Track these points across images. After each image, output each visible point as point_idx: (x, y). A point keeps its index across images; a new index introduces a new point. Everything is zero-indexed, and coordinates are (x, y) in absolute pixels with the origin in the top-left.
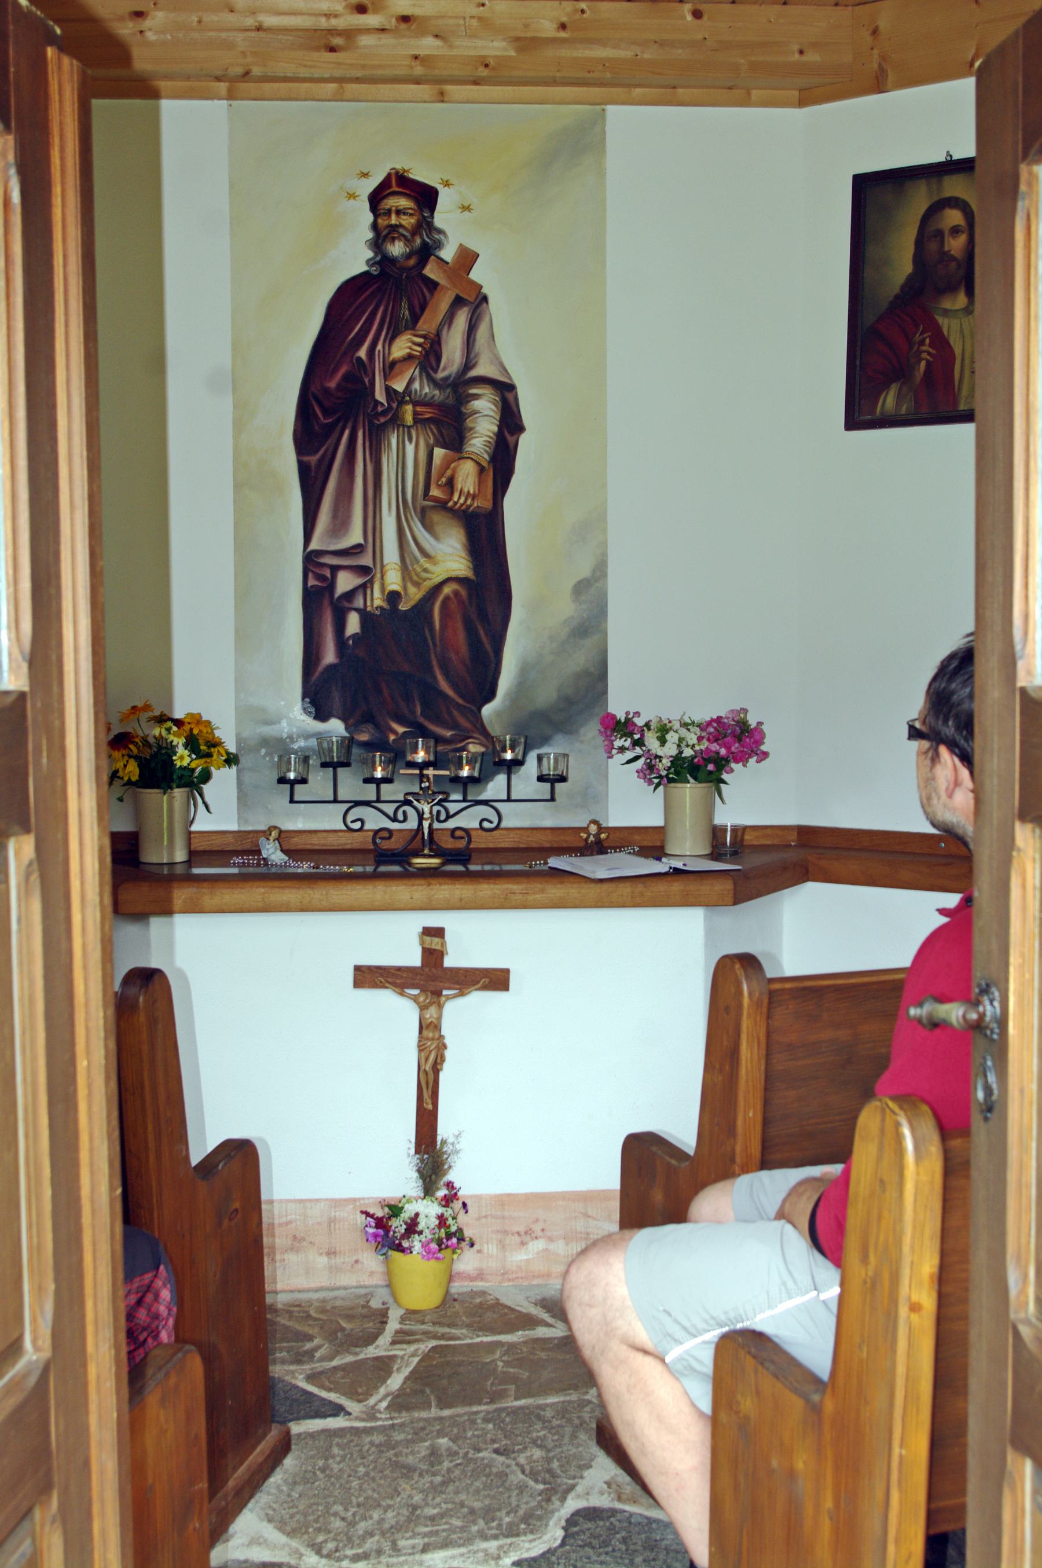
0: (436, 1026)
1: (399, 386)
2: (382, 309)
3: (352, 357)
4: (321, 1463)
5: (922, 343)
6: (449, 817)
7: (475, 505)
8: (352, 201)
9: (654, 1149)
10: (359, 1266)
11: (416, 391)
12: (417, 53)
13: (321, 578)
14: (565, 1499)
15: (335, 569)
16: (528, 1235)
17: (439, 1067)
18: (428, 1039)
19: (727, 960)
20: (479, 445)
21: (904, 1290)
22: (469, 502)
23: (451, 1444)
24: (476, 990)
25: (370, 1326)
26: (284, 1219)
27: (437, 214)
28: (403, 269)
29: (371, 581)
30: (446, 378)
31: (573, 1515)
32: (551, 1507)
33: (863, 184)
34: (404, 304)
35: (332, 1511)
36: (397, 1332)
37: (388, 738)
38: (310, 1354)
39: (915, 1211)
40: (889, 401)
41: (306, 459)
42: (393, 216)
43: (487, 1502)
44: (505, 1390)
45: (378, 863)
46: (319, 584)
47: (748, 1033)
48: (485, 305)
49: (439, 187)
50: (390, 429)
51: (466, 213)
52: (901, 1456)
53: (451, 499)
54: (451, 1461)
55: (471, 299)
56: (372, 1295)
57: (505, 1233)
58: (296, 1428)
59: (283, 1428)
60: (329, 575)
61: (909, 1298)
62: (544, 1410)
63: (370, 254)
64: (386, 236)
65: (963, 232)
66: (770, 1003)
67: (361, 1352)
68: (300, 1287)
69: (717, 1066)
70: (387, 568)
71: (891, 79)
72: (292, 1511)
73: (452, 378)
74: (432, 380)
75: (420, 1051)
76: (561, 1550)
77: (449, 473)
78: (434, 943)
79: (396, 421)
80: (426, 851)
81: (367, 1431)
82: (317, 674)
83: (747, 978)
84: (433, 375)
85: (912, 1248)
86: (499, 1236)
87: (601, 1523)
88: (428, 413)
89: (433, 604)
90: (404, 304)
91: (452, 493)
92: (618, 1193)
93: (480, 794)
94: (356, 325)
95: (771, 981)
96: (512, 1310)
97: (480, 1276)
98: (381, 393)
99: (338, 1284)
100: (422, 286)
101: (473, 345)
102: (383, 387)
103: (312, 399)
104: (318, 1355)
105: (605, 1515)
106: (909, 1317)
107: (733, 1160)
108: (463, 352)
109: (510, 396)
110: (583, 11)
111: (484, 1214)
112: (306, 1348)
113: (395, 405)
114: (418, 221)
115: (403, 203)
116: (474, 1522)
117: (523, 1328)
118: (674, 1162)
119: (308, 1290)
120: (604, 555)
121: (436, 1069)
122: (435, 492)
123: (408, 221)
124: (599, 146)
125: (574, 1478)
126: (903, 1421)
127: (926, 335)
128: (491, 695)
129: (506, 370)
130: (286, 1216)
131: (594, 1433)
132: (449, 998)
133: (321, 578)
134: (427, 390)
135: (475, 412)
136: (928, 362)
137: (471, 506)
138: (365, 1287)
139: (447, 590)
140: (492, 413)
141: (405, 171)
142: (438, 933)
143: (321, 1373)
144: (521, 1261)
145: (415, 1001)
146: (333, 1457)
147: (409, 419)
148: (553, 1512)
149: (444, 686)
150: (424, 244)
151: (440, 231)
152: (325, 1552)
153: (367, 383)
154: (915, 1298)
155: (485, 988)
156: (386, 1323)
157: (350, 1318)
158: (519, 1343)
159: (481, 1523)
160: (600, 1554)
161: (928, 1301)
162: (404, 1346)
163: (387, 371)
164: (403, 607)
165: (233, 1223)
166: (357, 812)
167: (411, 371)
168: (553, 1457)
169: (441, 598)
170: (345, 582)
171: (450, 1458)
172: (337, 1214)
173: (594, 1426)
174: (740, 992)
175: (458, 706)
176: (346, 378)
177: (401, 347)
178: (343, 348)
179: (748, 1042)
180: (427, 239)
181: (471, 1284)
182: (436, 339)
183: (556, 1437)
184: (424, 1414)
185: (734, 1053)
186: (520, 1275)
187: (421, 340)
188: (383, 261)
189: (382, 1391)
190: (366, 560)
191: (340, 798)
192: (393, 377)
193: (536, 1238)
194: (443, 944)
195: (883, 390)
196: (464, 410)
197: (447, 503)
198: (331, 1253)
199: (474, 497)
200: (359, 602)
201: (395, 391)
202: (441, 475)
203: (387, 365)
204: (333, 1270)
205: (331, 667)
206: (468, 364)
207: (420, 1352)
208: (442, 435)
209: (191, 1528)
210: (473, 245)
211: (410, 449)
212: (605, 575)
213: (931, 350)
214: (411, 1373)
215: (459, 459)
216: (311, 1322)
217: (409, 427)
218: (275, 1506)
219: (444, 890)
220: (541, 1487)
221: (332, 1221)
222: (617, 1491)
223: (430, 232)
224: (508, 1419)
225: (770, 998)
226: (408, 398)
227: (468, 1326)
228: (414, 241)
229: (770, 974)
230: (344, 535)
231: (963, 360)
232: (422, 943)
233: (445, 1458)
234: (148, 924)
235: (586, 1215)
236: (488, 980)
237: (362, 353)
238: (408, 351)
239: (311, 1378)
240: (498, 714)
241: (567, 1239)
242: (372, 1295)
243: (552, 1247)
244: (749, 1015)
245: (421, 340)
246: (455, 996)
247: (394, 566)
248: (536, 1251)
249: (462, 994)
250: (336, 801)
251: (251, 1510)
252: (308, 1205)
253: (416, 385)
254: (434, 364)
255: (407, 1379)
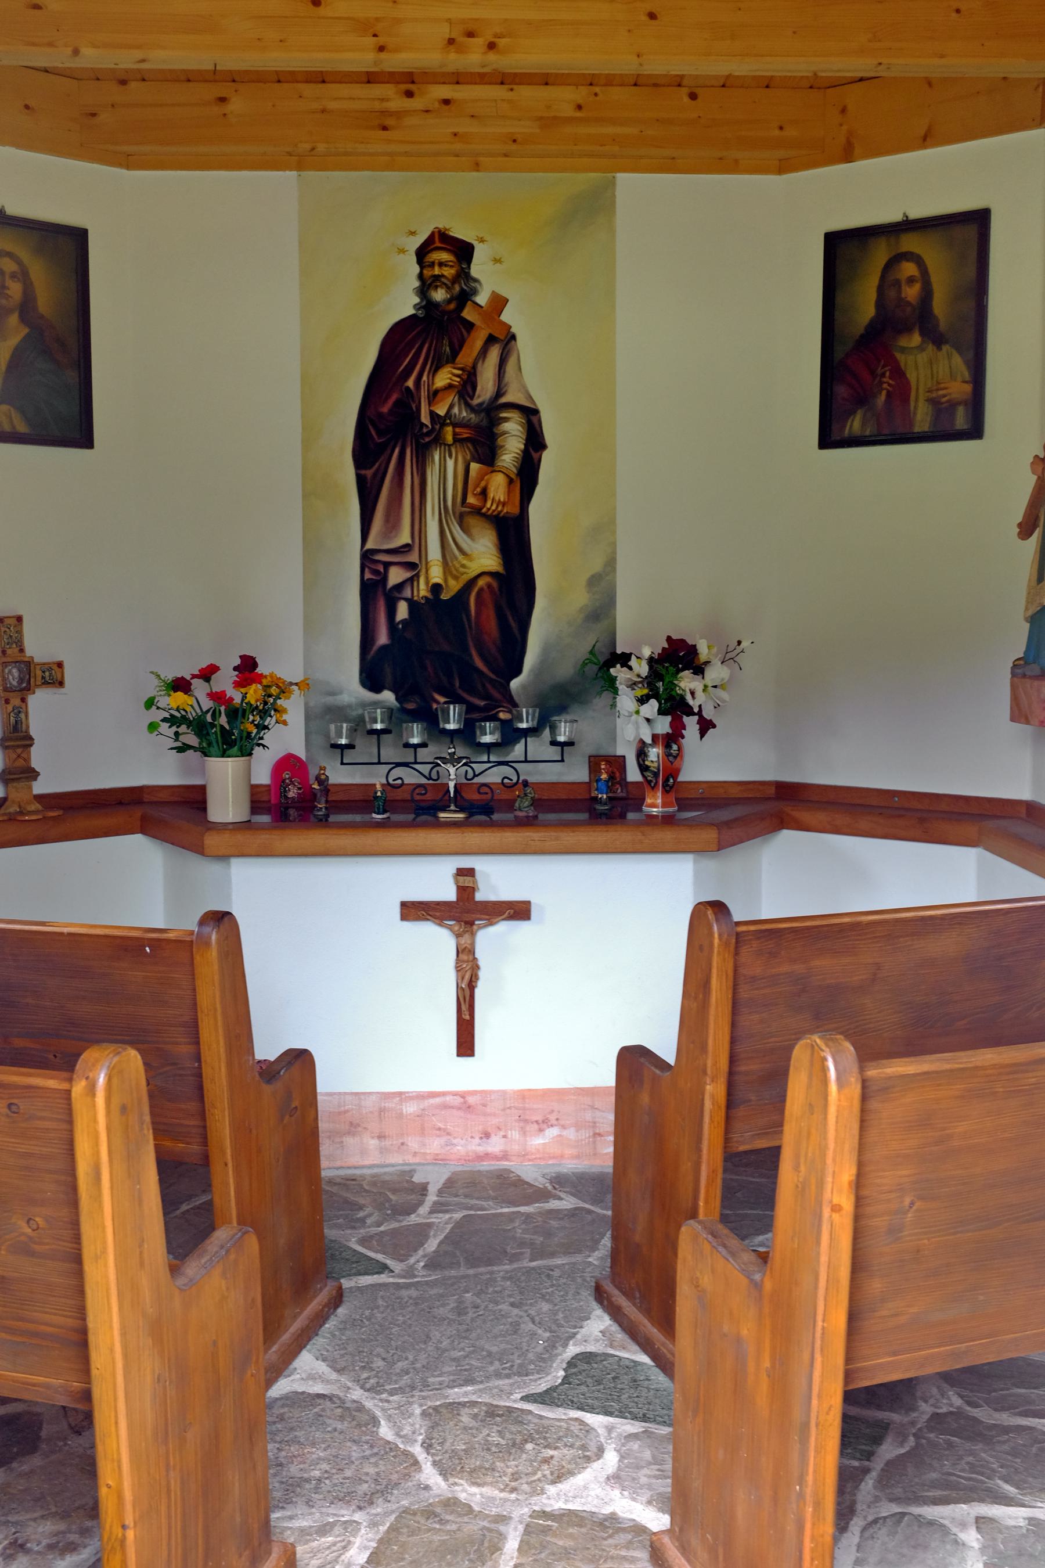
0: (471, 951)
1: (441, 411)
2: (426, 346)
3: (402, 385)
4: (367, 1313)
5: (883, 375)
6: (475, 776)
7: (505, 511)
8: (401, 255)
9: (642, 1060)
10: (405, 1147)
11: (455, 414)
12: (456, 130)
13: (376, 572)
14: (567, 1345)
15: (387, 565)
16: (544, 1124)
17: (474, 984)
18: (464, 961)
19: (702, 907)
20: (508, 460)
21: (827, 1195)
22: (500, 509)
23: (475, 1298)
24: (503, 920)
25: (413, 1198)
26: (342, 1109)
27: (472, 266)
28: (444, 312)
29: (417, 575)
30: (481, 404)
31: (573, 1358)
32: (556, 1352)
33: (835, 242)
34: (446, 342)
35: (374, 1353)
36: (435, 1203)
37: (431, 707)
38: (363, 1220)
39: (836, 1130)
40: (855, 425)
41: (363, 472)
42: (436, 268)
43: (503, 1346)
44: (522, 1254)
45: (418, 815)
46: (374, 577)
47: (718, 967)
48: (513, 342)
49: (475, 243)
50: (434, 446)
51: (498, 264)
52: (823, 1328)
53: (484, 506)
54: (474, 1313)
55: (502, 338)
56: (414, 1171)
57: (526, 1121)
58: (346, 1283)
59: (336, 1284)
60: (382, 570)
61: (831, 1202)
62: (99, 1540)
63: (417, 300)
64: (430, 285)
65: (917, 282)
66: (737, 942)
67: (404, 1220)
68: (356, 1164)
69: (693, 995)
70: (431, 564)
71: (857, 151)
72: (342, 1352)
73: (485, 406)
74: (468, 405)
75: (458, 971)
76: (561, 1387)
77: (483, 484)
78: (466, 881)
79: (438, 440)
80: (453, 807)
81: (407, 1286)
82: (372, 653)
83: (717, 920)
84: (470, 401)
85: (834, 1160)
86: (522, 1124)
87: (595, 1366)
88: (465, 433)
89: (469, 594)
90: (446, 342)
91: (485, 501)
92: (614, 1091)
93: (508, 754)
94: (405, 359)
95: (738, 924)
96: (531, 1185)
97: (505, 1156)
98: (425, 417)
99: (387, 1162)
100: (461, 326)
101: (503, 377)
102: (428, 412)
103: (367, 421)
104: (369, 1221)
105: (599, 1358)
106: (831, 1216)
107: (705, 1072)
108: (495, 381)
109: (534, 419)
110: (596, 95)
111: (508, 1106)
112: (358, 1216)
113: (437, 427)
114: (457, 271)
115: (445, 256)
116: (491, 1363)
117: (537, 1201)
118: (658, 1072)
119: (363, 1167)
120: (614, 552)
121: (472, 986)
122: (471, 500)
123: (449, 272)
124: (610, 207)
125: (575, 1327)
126: (825, 1299)
127: (887, 369)
128: (518, 671)
129: (531, 397)
130: (344, 1106)
131: (593, 1289)
132: (481, 927)
133: (376, 572)
134: (464, 414)
135: (504, 433)
136: (888, 391)
137: (501, 511)
138: (409, 1164)
139: (481, 582)
140: (519, 434)
141: (446, 230)
142: (470, 872)
143: (372, 1237)
144: (539, 1144)
145: (451, 930)
146: (378, 1307)
147: (449, 438)
148: (557, 1355)
149: (479, 663)
150: (462, 291)
151: (476, 280)
152: (368, 1386)
153: (414, 409)
154: (835, 1201)
155: (511, 918)
156: (426, 1195)
157: (394, 1191)
158: (534, 1214)
159: (497, 1363)
160: (594, 1391)
161: (847, 1203)
162: (441, 1215)
163: (431, 399)
164: (445, 596)
165: (293, 1118)
166: (398, 772)
167: (451, 398)
168: (558, 1310)
169: (476, 590)
170: (396, 576)
171: (474, 1310)
172: (386, 1105)
173: (593, 1284)
174: (711, 934)
175: (491, 680)
176: (398, 403)
177: (444, 378)
178: (394, 379)
179: (718, 975)
180: (465, 288)
181: (497, 1163)
182: (472, 371)
183: (562, 1293)
184: (453, 1273)
185: (706, 984)
186: (538, 1156)
187: (459, 372)
188: (427, 305)
189: (420, 1252)
190: (413, 557)
191: (382, 761)
192: (436, 404)
193: (552, 1126)
194: (475, 882)
195: (848, 419)
196: (495, 430)
197: (482, 509)
198: (381, 1137)
199: (504, 504)
200: (407, 593)
201: (438, 415)
202: (477, 486)
203: (431, 393)
204: (383, 1151)
205: (384, 647)
206: (499, 393)
207: (453, 1220)
208: (477, 451)
209: (249, 1373)
210: (504, 292)
211: (450, 463)
212: (614, 570)
213: (891, 382)
214: (446, 1237)
215: (492, 472)
216: (364, 1194)
217: (449, 446)
218: (328, 1347)
219: (475, 837)
220: (547, 1334)
221: (382, 1111)
222: (610, 1339)
223: (468, 281)
224: (523, 1278)
225: (737, 939)
226: (448, 421)
227: (494, 1198)
228: (454, 288)
229: (737, 917)
230: (395, 536)
231: (917, 389)
232: (456, 882)
233: (469, 1310)
234: (229, 864)
235: (593, 1107)
236: (512, 911)
237: (410, 383)
238: (449, 381)
239: (364, 1241)
240: (524, 687)
241: (578, 1126)
242: (414, 1171)
243: (565, 1133)
244: (719, 953)
245: (459, 372)
246: (485, 926)
247: (436, 562)
248: (551, 1136)
249: (492, 924)
250: (379, 763)
251: (309, 1351)
252: (362, 1097)
253: (456, 410)
254: (471, 393)
255: (441, 1243)
